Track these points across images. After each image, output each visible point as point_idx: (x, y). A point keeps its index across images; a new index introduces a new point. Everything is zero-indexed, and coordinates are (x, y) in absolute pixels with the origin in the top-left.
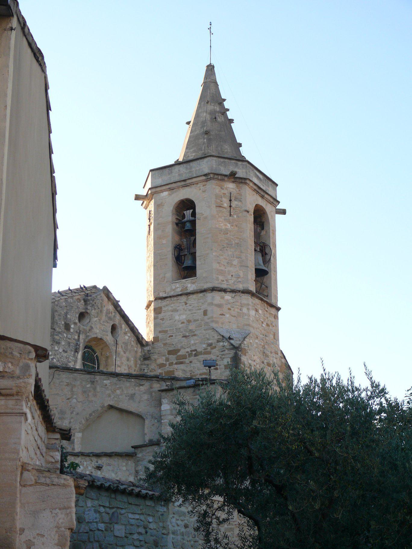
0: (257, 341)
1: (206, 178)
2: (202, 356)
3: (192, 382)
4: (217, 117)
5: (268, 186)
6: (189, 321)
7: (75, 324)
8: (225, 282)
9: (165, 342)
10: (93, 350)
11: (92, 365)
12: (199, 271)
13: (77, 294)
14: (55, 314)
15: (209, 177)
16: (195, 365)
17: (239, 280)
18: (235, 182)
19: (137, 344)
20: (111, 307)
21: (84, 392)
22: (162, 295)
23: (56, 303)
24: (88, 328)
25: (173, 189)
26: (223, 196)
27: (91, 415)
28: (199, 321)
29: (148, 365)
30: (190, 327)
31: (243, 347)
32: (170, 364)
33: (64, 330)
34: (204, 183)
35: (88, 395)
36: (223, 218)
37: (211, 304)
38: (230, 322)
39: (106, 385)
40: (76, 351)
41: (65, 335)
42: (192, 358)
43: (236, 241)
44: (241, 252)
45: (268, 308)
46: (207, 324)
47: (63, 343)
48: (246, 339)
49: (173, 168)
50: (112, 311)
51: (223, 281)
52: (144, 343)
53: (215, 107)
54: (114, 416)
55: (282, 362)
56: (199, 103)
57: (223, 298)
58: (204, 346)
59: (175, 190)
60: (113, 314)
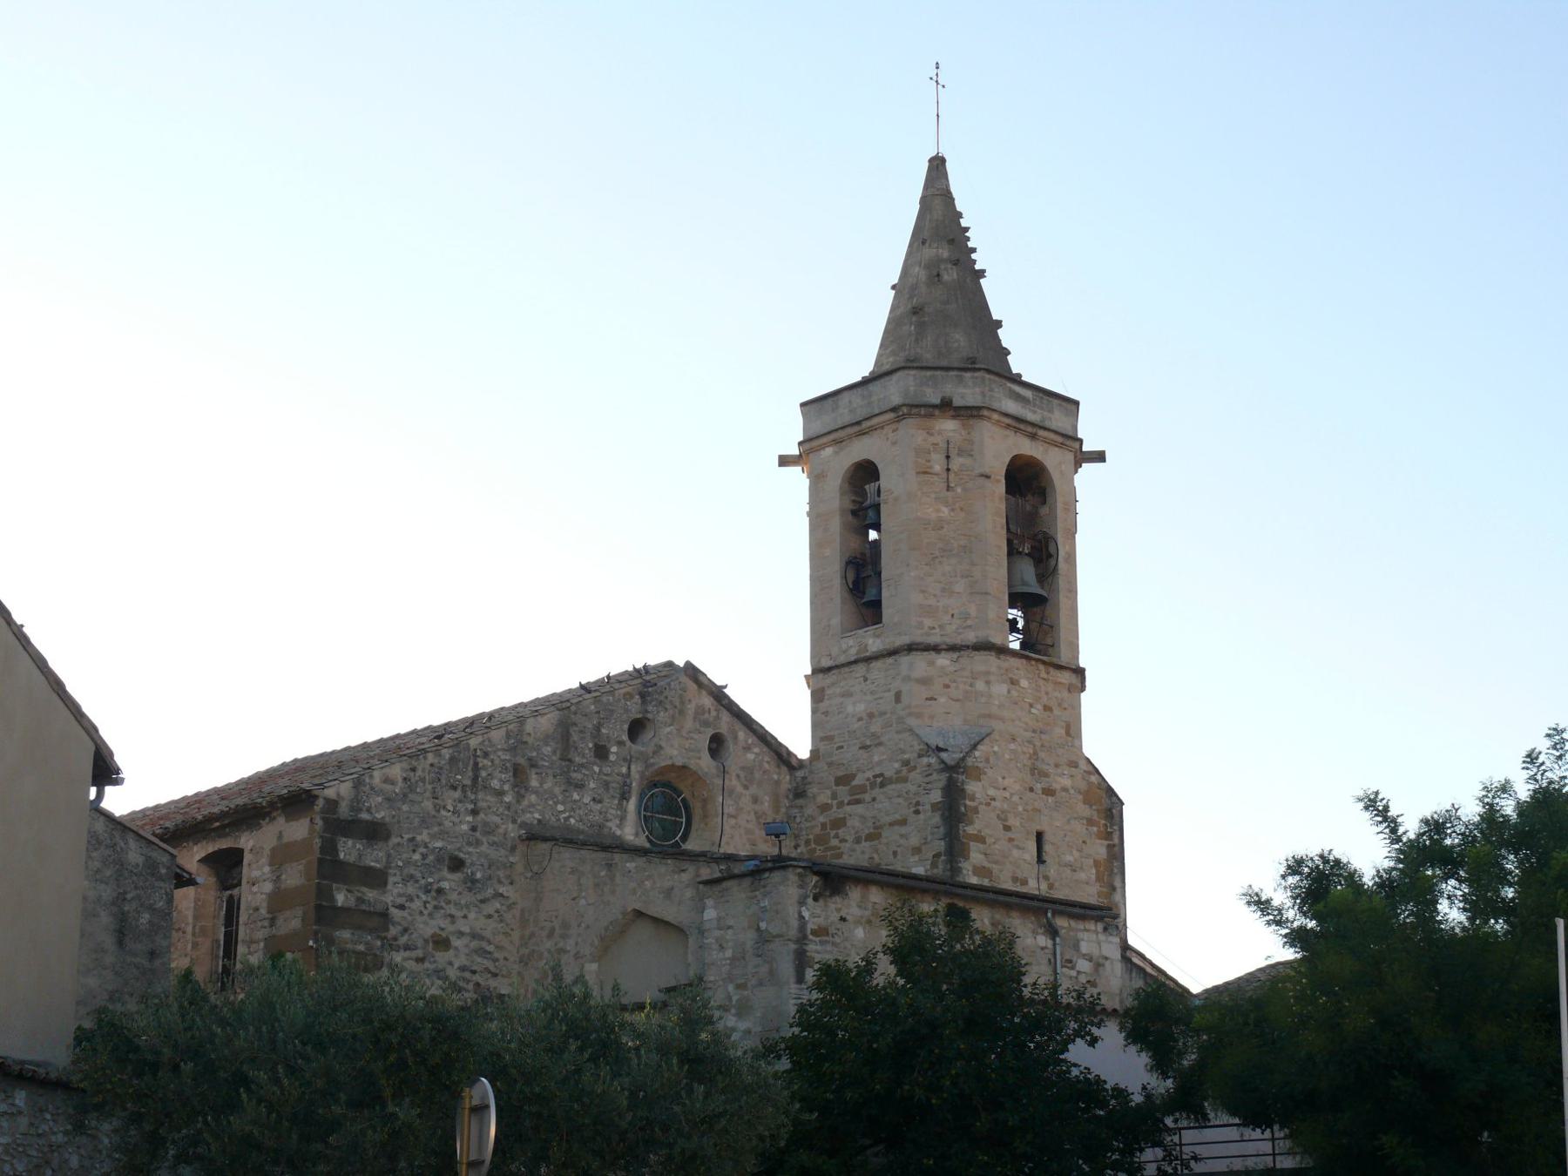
0: (1012, 746)
1: (896, 416)
2: (893, 786)
3: (751, 865)
4: (942, 272)
5: (1051, 411)
6: (871, 716)
7: (620, 743)
8: (938, 630)
9: (829, 760)
10: (675, 790)
11: (673, 818)
12: (887, 611)
13: (623, 685)
14: (571, 731)
15: (901, 413)
16: (880, 806)
17: (969, 622)
18: (959, 416)
19: (778, 767)
20: (707, 701)
21: (597, 885)
22: (826, 663)
23: (573, 708)
24: (650, 749)
25: (841, 442)
26: (932, 449)
27: (606, 929)
28: (888, 715)
29: (802, 807)
30: (873, 728)
31: (970, 764)
32: (840, 805)
33: (593, 759)
34: (894, 426)
35: (602, 891)
36: (933, 496)
37: (907, 679)
38: (949, 713)
39: (630, 872)
40: (624, 796)
41: (596, 769)
42: (877, 791)
43: (962, 543)
44: (973, 564)
45: (1048, 673)
46: (900, 720)
47: (592, 785)
48: (979, 747)
49: (840, 397)
50: (709, 709)
51: (934, 628)
52: (794, 762)
53: (940, 251)
54: (643, 931)
55: (1090, 784)
56: (911, 245)
57: (931, 663)
58: (897, 765)
59: (844, 443)
60: (714, 713)
